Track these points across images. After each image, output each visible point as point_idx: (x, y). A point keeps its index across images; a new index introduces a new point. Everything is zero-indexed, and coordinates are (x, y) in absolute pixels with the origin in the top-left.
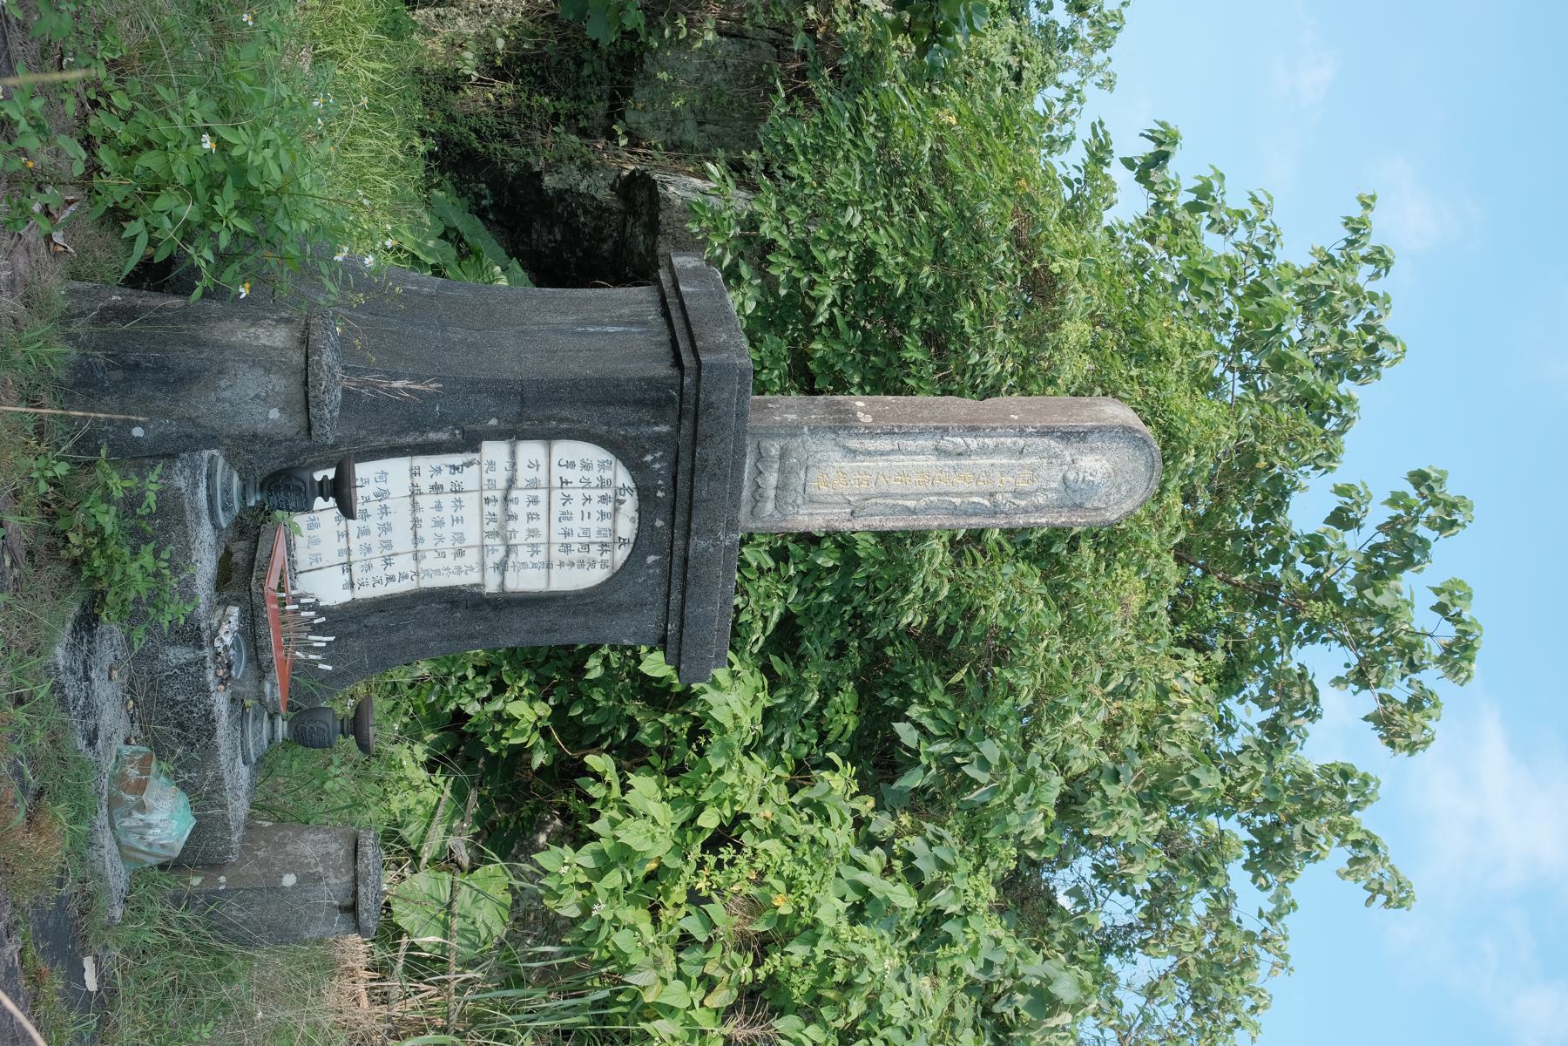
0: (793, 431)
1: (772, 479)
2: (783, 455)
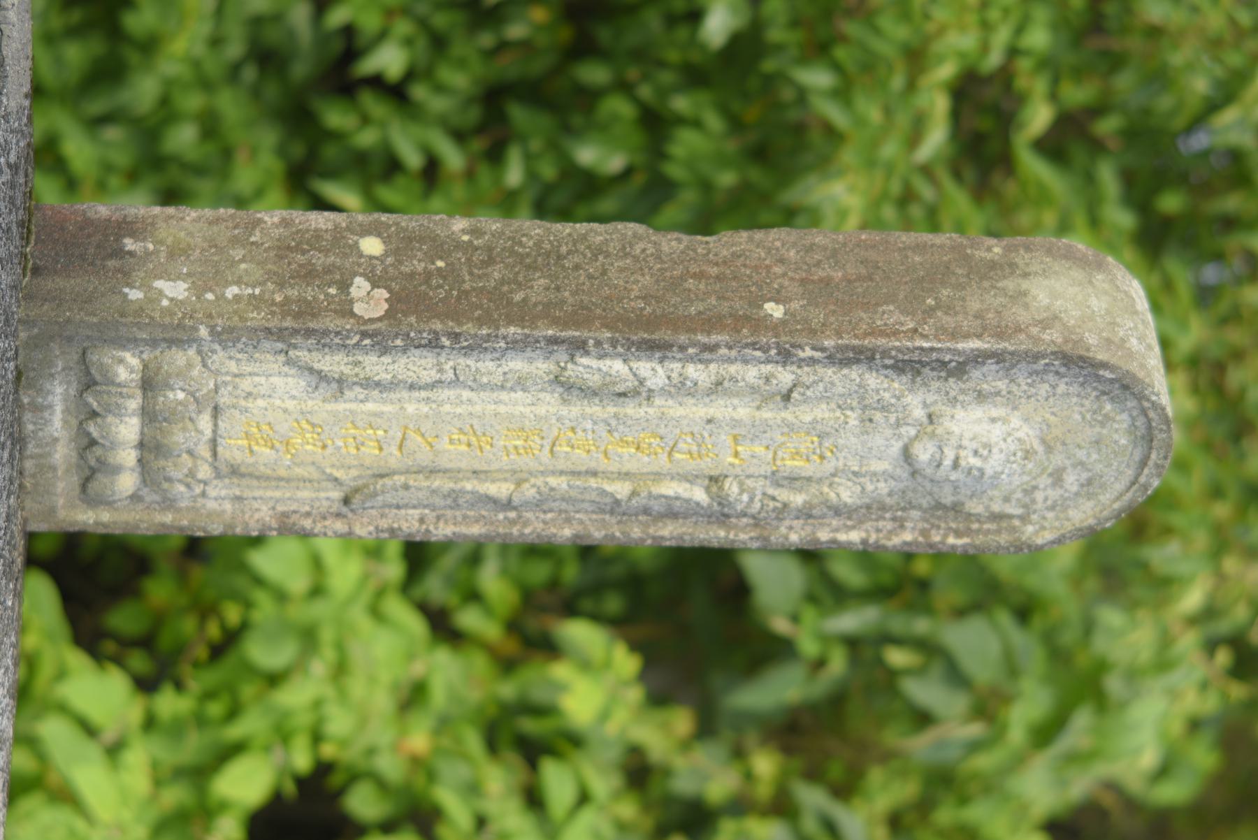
0: (174, 332)
1: (128, 429)
2: (149, 384)
